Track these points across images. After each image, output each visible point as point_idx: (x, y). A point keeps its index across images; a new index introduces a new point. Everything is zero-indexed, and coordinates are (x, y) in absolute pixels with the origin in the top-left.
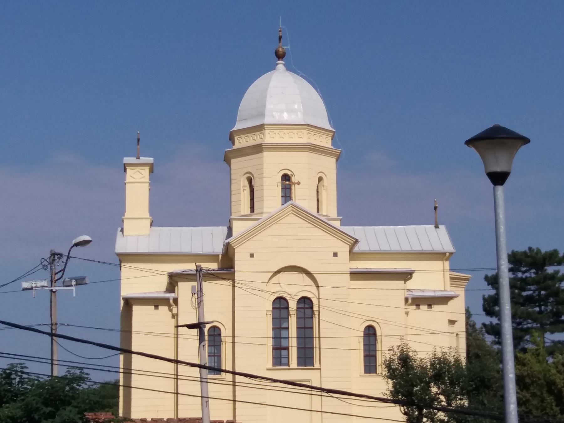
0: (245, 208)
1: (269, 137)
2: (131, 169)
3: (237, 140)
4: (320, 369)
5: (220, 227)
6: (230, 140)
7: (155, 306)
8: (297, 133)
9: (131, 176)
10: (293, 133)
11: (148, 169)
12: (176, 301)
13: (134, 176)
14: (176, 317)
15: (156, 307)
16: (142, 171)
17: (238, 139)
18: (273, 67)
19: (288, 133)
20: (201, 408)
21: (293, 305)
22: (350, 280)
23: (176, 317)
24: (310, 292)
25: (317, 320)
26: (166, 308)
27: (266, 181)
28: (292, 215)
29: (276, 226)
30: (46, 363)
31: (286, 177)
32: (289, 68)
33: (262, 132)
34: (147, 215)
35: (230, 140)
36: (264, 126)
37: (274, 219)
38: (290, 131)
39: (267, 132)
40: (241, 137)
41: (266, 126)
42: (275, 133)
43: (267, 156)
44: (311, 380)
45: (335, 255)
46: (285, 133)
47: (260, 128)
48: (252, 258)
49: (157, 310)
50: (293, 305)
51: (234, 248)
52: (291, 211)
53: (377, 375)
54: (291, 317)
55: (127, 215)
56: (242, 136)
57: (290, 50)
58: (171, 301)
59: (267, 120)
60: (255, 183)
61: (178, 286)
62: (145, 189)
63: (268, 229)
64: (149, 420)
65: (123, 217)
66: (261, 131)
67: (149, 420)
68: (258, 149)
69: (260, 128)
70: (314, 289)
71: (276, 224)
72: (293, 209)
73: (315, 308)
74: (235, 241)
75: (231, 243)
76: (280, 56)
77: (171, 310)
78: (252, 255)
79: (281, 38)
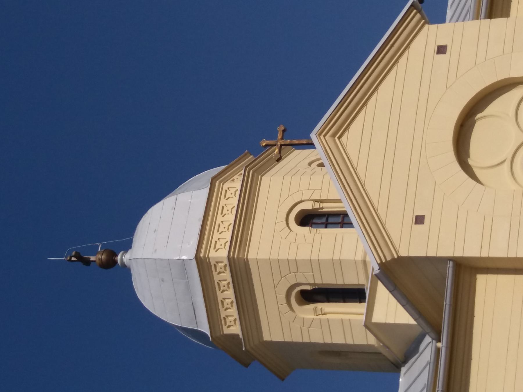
3: (231, 328)
5: (401, 380)
6: (246, 365)
8: (227, 200)
10: (225, 206)
18: (126, 271)
19: (223, 216)
28: (344, 139)
29: (361, 172)
30: (357, 220)
32: (127, 246)
33: (212, 263)
35: (246, 365)
36: (200, 257)
39: (213, 254)
40: (225, 319)
41: (202, 255)
42: (219, 239)
45: (441, 50)
46: (222, 222)
48: (427, 220)
51: (396, 257)
57: (177, 330)
66: (211, 266)
75: (384, 261)
78: (419, 220)
79: (79, 253)
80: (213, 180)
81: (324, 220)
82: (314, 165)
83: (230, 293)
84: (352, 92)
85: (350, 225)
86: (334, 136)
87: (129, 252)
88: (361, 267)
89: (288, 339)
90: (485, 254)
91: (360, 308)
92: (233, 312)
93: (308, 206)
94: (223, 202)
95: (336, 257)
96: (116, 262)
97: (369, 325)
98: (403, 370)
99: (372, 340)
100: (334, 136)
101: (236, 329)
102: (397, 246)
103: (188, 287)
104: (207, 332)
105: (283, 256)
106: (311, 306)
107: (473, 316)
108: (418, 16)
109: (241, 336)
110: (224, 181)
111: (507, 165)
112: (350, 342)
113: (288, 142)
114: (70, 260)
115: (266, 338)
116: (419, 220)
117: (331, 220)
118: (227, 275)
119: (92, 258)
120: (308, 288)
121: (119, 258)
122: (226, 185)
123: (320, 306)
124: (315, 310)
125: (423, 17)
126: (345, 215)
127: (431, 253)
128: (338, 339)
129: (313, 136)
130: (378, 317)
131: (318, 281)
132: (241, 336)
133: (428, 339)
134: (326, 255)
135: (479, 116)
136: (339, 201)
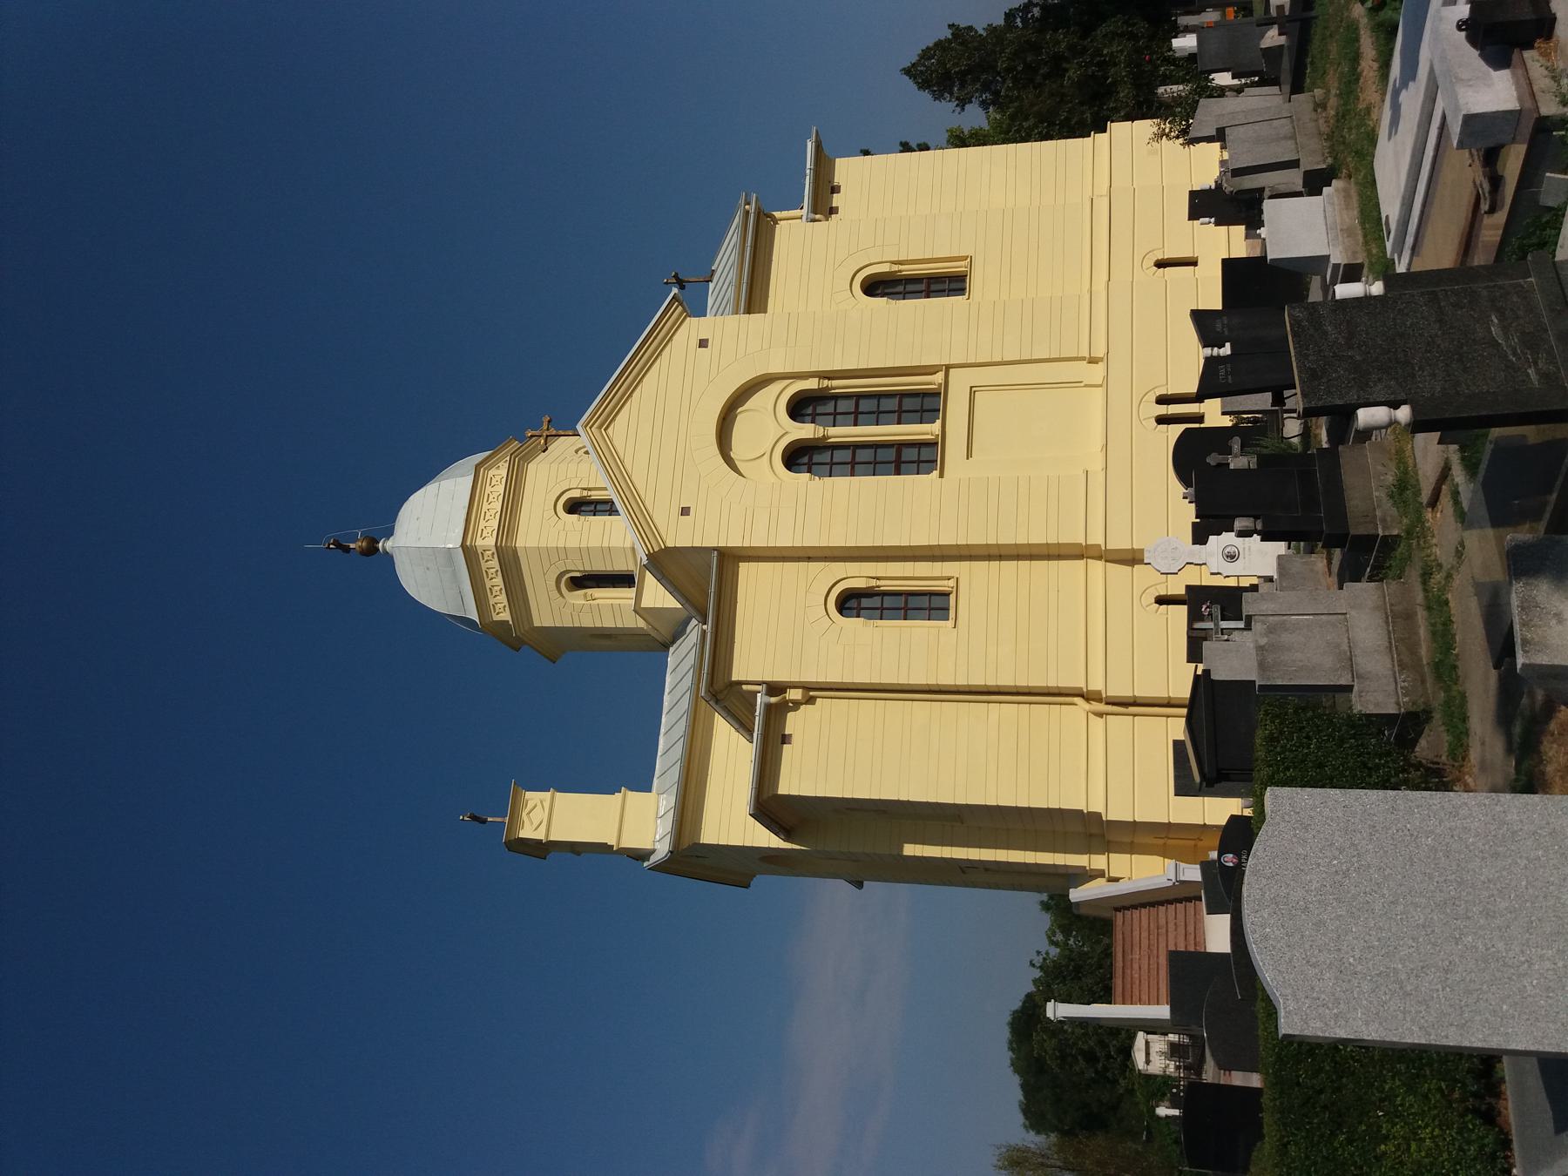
1: (486, 540)
2: (523, 828)
4: (948, 367)
7: (783, 742)
9: (536, 829)
11: (527, 793)
12: (775, 689)
13: (536, 823)
14: (811, 693)
15: (785, 739)
16: (530, 806)
17: (498, 614)
18: (389, 558)
20: (1044, 563)
21: (806, 431)
22: (765, 312)
23: (811, 693)
25: (835, 383)
26: (791, 717)
28: (610, 430)
32: (389, 533)
37: (611, 463)
38: (485, 500)
39: (479, 542)
43: (527, 538)
44: (971, 387)
45: (703, 343)
47: (470, 554)
49: (794, 739)
50: (806, 431)
52: (601, 432)
53: (955, 592)
54: (830, 438)
55: (612, 841)
56: (492, 602)
58: (773, 700)
59: (454, 542)
60: (579, 567)
61: (740, 683)
63: (633, 478)
65: (615, 849)
68: (509, 561)
69: (470, 554)
71: (626, 464)
72: (595, 426)
73: (812, 384)
74: (648, 544)
76: (371, 550)
77: (797, 705)
78: (685, 511)
80: (478, 467)
81: (592, 508)
83: (499, 581)
86: (600, 427)
91: (630, 593)
92: (503, 598)
93: (576, 494)
95: (605, 545)
97: (638, 610)
99: (641, 624)
100: (600, 427)
101: (505, 616)
103: (455, 575)
104: (474, 616)
105: (552, 544)
106: (582, 592)
107: (733, 642)
108: (680, 308)
109: (511, 623)
111: (767, 457)
112: (620, 625)
114: (328, 547)
115: (537, 623)
116: (685, 511)
117: (599, 507)
118: (495, 563)
119: (352, 546)
120: (578, 574)
121: (380, 545)
122: (491, 473)
123: (589, 591)
124: (585, 595)
125: (684, 310)
127: (697, 544)
128: (608, 623)
129: (579, 427)
133: (694, 622)
134: (594, 542)
136: (605, 489)
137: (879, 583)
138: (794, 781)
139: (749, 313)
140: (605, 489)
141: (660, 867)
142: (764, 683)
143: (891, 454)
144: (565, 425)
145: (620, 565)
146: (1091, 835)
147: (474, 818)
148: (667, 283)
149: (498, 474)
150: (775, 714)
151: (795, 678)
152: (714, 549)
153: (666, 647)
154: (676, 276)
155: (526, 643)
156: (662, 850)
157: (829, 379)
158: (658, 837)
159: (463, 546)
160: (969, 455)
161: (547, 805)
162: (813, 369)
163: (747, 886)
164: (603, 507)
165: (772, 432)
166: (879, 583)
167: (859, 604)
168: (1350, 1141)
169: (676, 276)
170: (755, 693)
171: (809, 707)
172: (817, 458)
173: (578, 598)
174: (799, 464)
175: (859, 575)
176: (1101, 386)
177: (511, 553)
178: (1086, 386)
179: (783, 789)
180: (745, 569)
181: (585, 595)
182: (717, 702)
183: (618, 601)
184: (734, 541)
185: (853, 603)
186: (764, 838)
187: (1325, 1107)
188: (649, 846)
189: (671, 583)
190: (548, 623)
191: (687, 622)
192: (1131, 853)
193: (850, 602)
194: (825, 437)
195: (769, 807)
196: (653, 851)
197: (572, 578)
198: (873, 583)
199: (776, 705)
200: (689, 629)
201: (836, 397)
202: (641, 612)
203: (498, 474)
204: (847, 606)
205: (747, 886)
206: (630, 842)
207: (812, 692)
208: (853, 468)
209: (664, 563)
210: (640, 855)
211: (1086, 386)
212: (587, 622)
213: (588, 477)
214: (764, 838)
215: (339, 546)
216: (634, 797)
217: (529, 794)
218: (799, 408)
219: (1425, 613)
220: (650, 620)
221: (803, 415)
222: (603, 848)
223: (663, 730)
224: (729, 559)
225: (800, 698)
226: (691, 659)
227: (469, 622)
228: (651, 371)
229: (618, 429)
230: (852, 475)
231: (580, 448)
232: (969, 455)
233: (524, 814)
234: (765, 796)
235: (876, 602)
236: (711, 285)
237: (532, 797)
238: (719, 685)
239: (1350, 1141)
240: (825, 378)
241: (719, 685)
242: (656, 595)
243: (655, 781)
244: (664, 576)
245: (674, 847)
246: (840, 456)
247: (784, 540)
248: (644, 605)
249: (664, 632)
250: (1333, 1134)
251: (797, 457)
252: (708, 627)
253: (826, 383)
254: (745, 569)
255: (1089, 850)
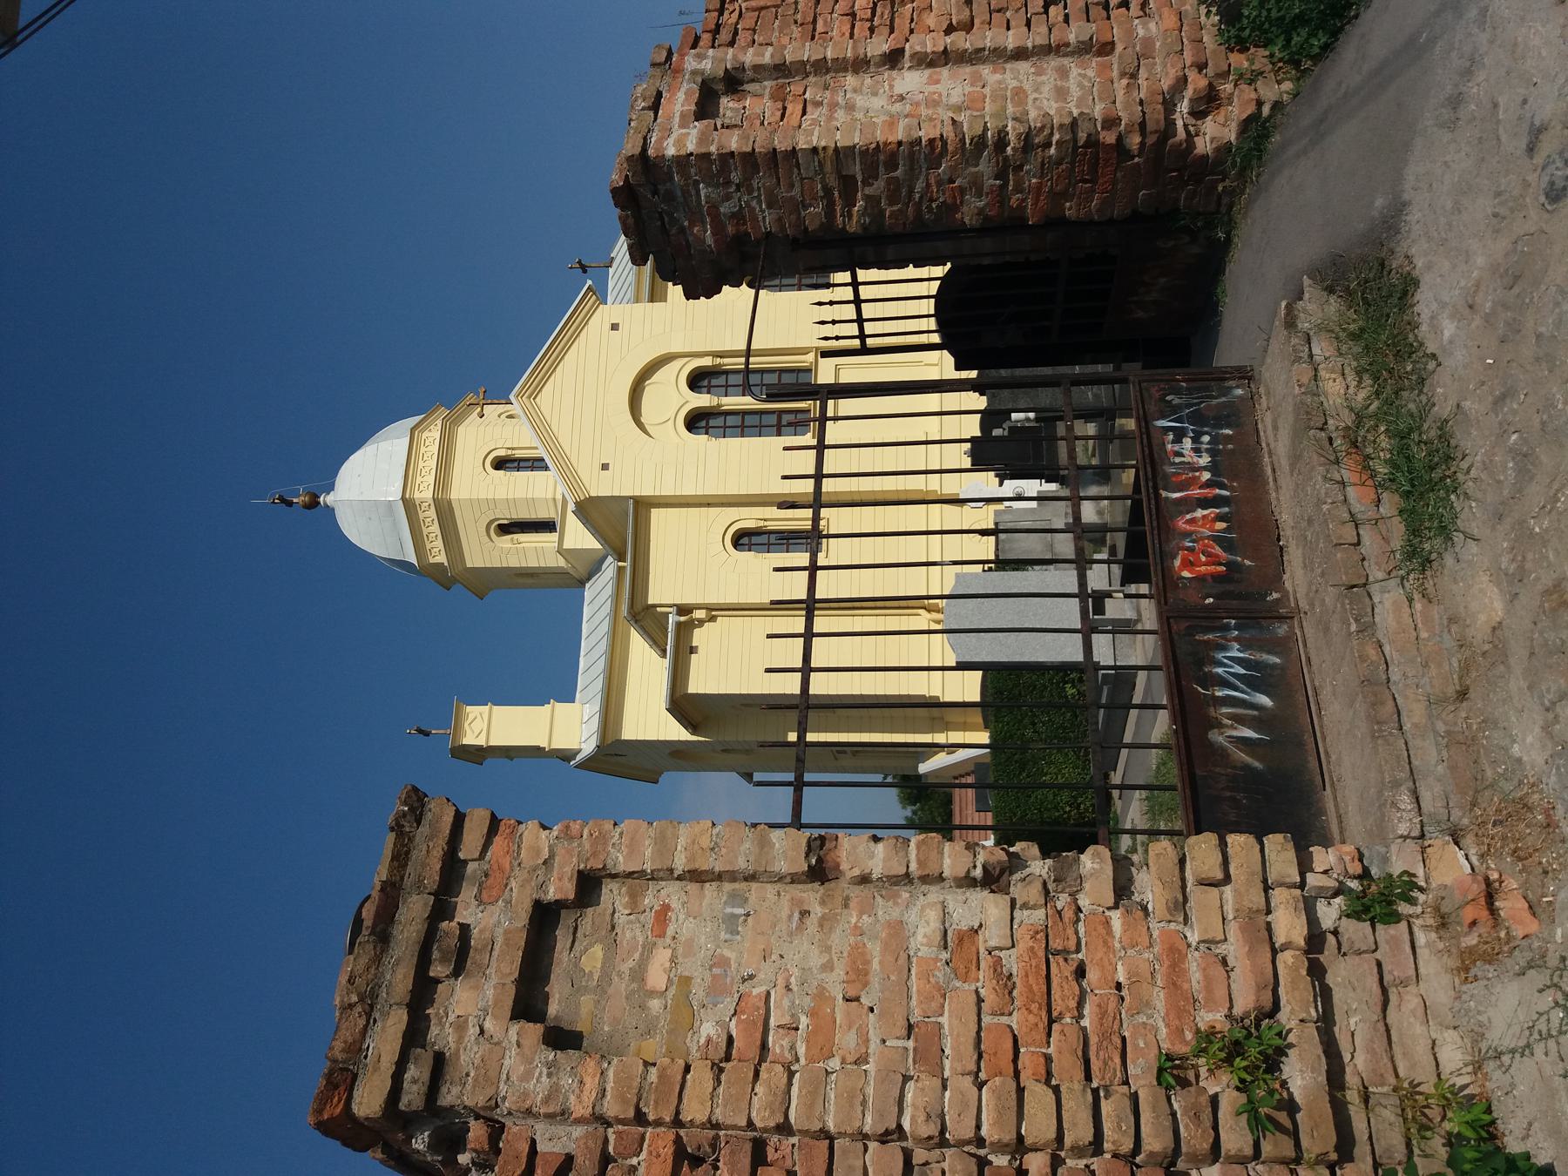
0: (547, 540)
1: (424, 492)
12: (683, 610)
15: (693, 650)
16: (471, 717)
18: (330, 511)
21: (703, 400)
22: (666, 301)
24: (677, 373)
25: (726, 361)
26: (697, 631)
27: (501, 494)
28: (537, 400)
31: (501, 464)
32: (330, 488)
34: (547, 707)
37: (540, 427)
39: (417, 495)
43: (460, 491)
45: (615, 327)
47: (410, 506)
49: (700, 650)
50: (703, 400)
55: (543, 743)
58: (682, 619)
59: (394, 493)
60: (506, 516)
61: (655, 606)
62: (501, 712)
64: (726, 288)
67: (726, 288)
69: (410, 506)
70: (677, 364)
73: (707, 362)
76: (313, 503)
77: (701, 622)
78: (605, 467)
80: (413, 430)
81: (516, 464)
82: (503, 416)
83: (435, 528)
84: (864, 771)
85: (546, 468)
86: (529, 397)
87: (332, 493)
88: (551, 504)
89: (488, 565)
90: (657, 494)
91: (554, 537)
92: (439, 543)
93: (502, 453)
94: (423, 449)
95: (530, 496)
96: (319, 503)
97: (560, 551)
98: (587, 585)
99: (562, 563)
100: (529, 397)
101: (441, 558)
102: (588, 488)
103: (395, 524)
104: (414, 561)
105: (482, 496)
106: (509, 537)
107: (648, 573)
108: (594, 297)
109: (446, 564)
110: (422, 431)
111: (671, 423)
112: (543, 565)
113: (489, 401)
114: (273, 502)
115: (469, 565)
116: (605, 467)
117: (522, 464)
118: (432, 513)
119: (295, 500)
120: (506, 522)
121: (321, 499)
122: (425, 435)
123: (515, 536)
124: (512, 539)
125: (598, 299)
126: (542, 460)
127: (616, 493)
128: (533, 563)
129: (512, 397)
130: (569, 544)
131: (514, 516)
132: (446, 564)
133: (610, 559)
134: (520, 494)
135: (647, 382)
136: (536, 448)
137: (766, 523)
138: (701, 682)
139: (652, 301)
140: (536, 448)
141: (584, 765)
142: (675, 605)
143: (773, 419)
144: (498, 393)
145: (543, 514)
146: (934, 719)
147: (420, 731)
148: (571, 268)
149: (432, 436)
150: (684, 630)
151: (700, 601)
152: (631, 497)
153: (582, 583)
154: (579, 262)
155: (459, 581)
156: (588, 747)
157: (721, 357)
158: (583, 739)
159: (403, 498)
160: (777, 570)
161: (486, 717)
162: (709, 349)
163: (656, 782)
164: (537, 464)
165: (676, 401)
166: (766, 523)
167: (750, 540)
168: (1028, 776)
169: (579, 262)
170: (667, 614)
171: (711, 624)
172: (712, 423)
173: (506, 541)
174: (698, 428)
175: (750, 518)
176: (937, 365)
177: (446, 504)
178: (926, 365)
179: (692, 689)
180: (656, 513)
181: (512, 539)
182: (636, 622)
183: (541, 545)
184: (647, 491)
185: (745, 540)
186: (676, 732)
187: (1016, 762)
188: (575, 746)
189: (594, 528)
190: (479, 564)
191: (605, 558)
192: (965, 730)
193: (743, 539)
194: (719, 406)
195: (683, 705)
196: (580, 751)
197: (499, 525)
198: (761, 523)
199: (684, 622)
200: (604, 567)
201: (727, 372)
202: (564, 553)
203: (432, 436)
204: (741, 542)
205: (656, 782)
206: (559, 744)
207: (714, 611)
208: (742, 431)
209: (589, 510)
210: (565, 756)
211: (926, 365)
212: (514, 562)
213: (518, 438)
214: (676, 732)
215: (282, 500)
216: (561, 708)
217: (469, 708)
218: (697, 381)
219: (1302, 571)
220: (572, 561)
221: (700, 387)
222: (536, 751)
223: (582, 653)
224: (643, 506)
225: (704, 616)
226: (609, 590)
227: (403, 564)
228: (570, 352)
229: (545, 398)
230: (742, 436)
231: (502, 414)
232: (777, 570)
233: (466, 725)
234: (678, 695)
235: (764, 539)
236: (611, 271)
237: (472, 711)
238: (638, 607)
239: (1028, 776)
240: (718, 356)
241: (638, 607)
242: (578, 536)
243: (578, 695)
244: (587, 521)
245: (601, 743)
246: (731, 420)
247: (688, 490)
248: (566, 546)
249: (582, 572)
250: (1020, 774)
251: (696, 421)
252: (627, 564)
253: (718, 360)
254: (656, 513)
255: (932, 730)
